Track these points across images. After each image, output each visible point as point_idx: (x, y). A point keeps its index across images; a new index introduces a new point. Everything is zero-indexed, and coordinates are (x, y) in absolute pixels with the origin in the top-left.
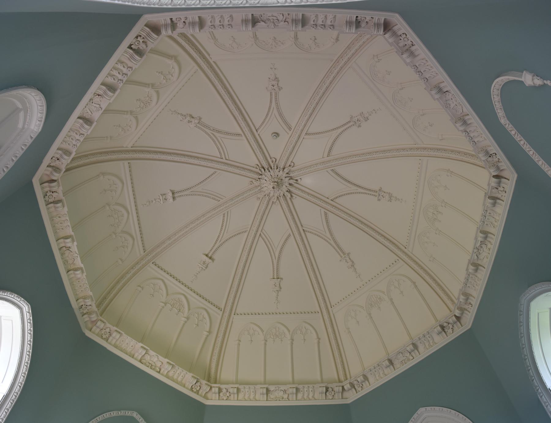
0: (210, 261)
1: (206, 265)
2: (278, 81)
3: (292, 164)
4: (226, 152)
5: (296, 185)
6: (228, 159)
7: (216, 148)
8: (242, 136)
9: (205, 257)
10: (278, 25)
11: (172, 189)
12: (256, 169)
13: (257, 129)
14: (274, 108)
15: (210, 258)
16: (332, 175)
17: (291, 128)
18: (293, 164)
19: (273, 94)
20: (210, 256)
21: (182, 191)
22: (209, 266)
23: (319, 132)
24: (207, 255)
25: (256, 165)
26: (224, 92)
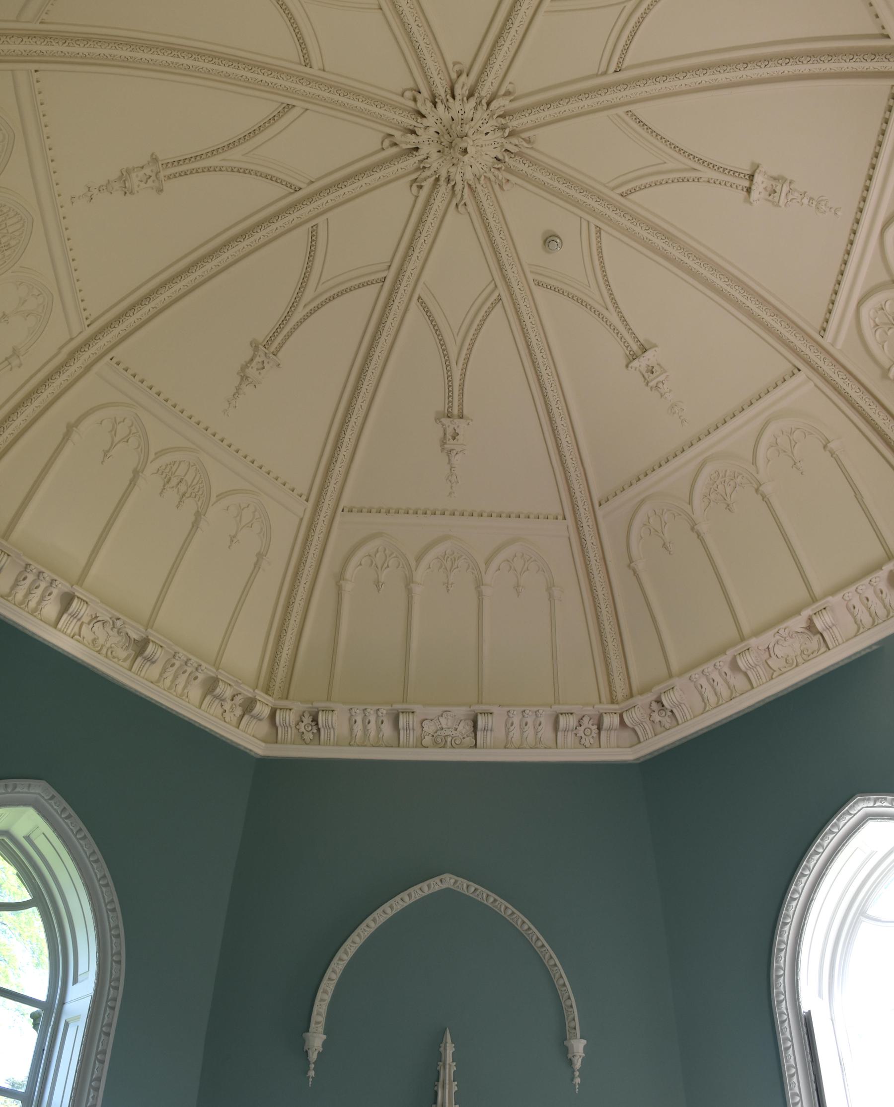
0: (758, 178)
1: (774, 183)
2: (244, 368)
3: (387, 143)
4: (480, 300)
5: (425, 93)
6: (493, 282)
7: (476, 345)
8: (419, 298)
9: (755, 195)
10: (111, 618)
11: (625, 363)
12: (468, 203)
13: (381, 284)
14: (303, 305)
15: (751, 177)
16: (284, 129)
17: (311, 229)
18: (384, 143)
19: (273, 349)
20: (746, 183)
21: (694, 158)
22: (775, 174)
23: (258, 178)
24: (749, 190)
25: (458, 212)
26: (306, 566)
